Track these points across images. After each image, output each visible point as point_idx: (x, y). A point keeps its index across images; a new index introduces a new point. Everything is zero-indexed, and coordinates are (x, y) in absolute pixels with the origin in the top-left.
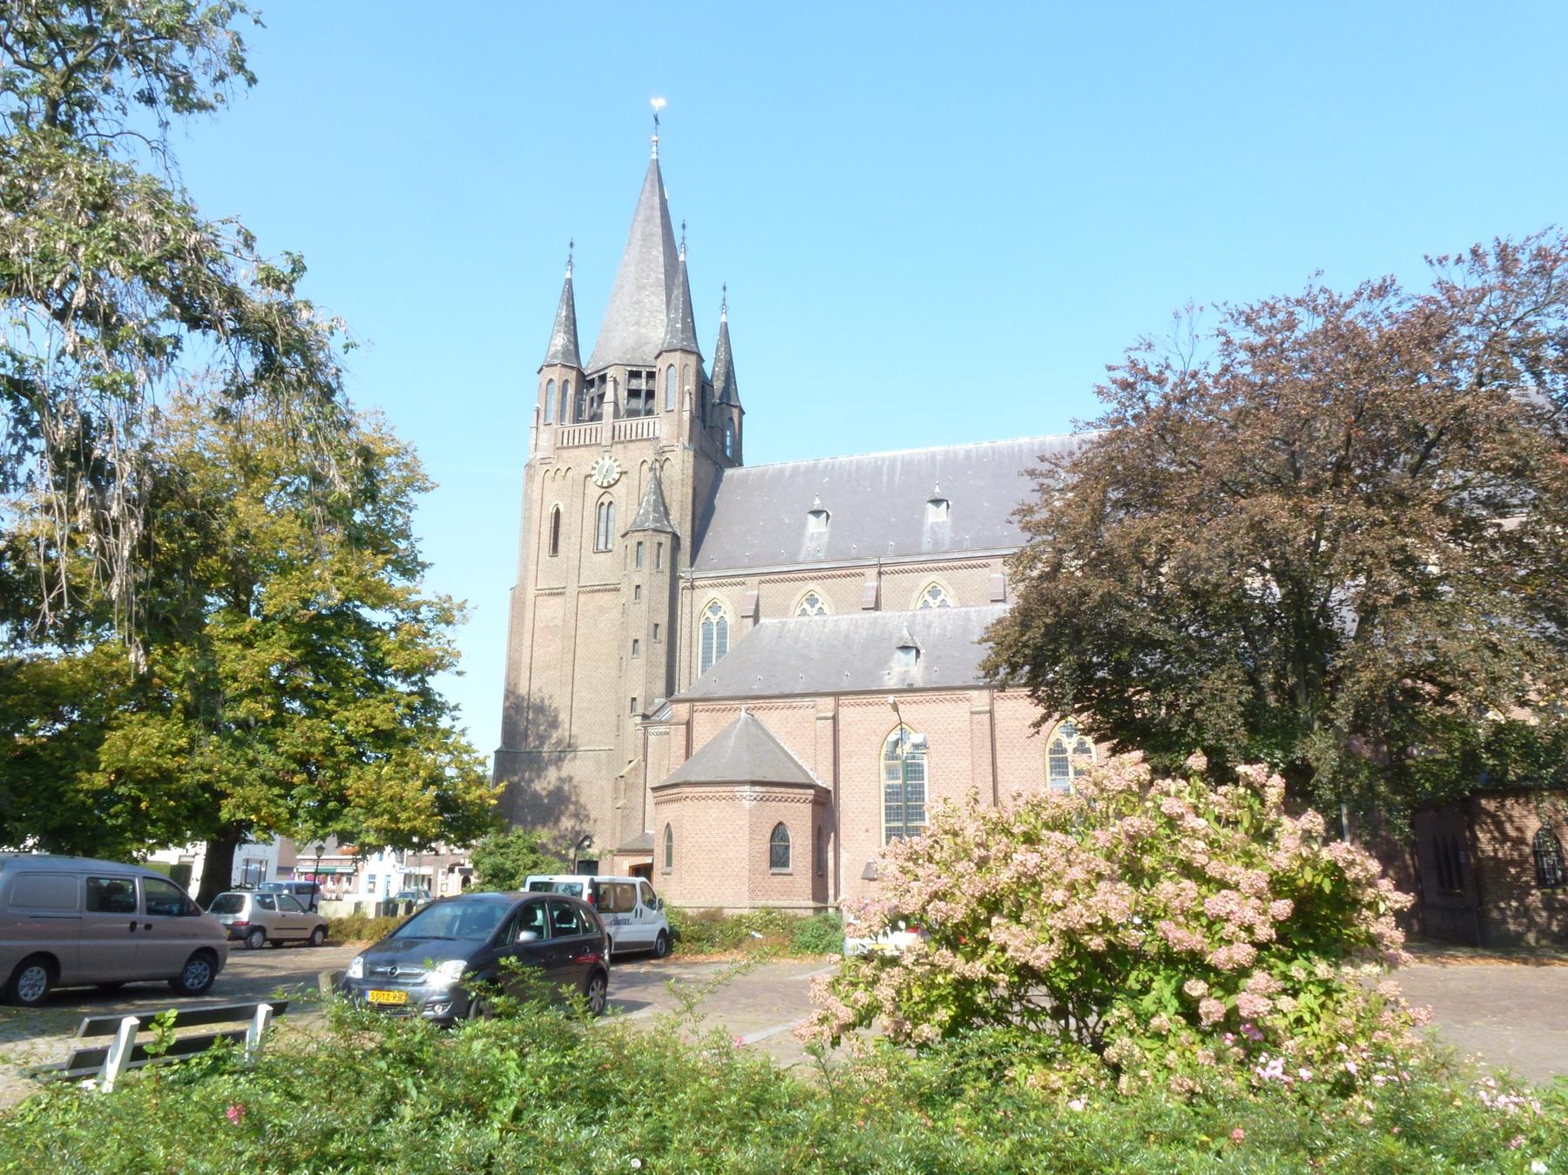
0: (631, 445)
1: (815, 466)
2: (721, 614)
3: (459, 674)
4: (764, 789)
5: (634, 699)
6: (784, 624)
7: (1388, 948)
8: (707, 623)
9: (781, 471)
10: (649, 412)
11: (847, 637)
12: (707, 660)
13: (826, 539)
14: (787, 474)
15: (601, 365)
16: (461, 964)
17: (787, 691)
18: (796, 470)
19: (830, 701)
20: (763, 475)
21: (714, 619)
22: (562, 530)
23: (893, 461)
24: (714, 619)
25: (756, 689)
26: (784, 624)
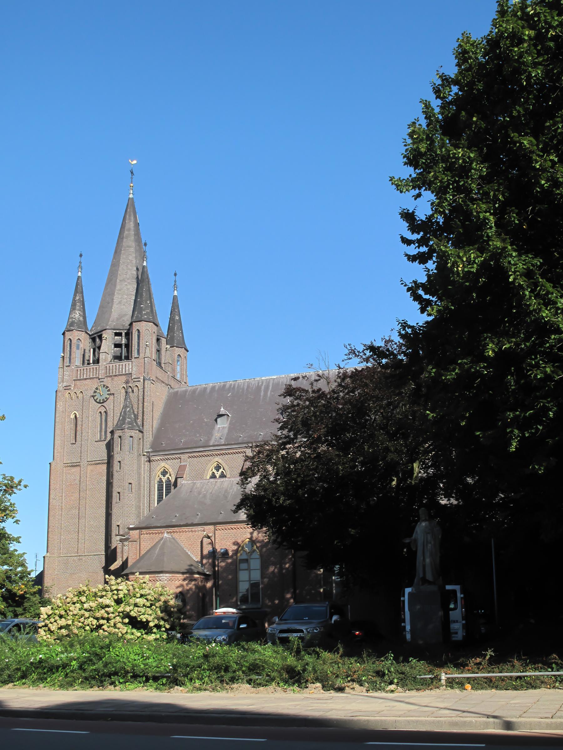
0: (116, 378)
1: (224, 386)
2: (168, 476)
3: (17, 522)
4: (171, 575)
5: (118, 526)
6: (195, 484)
7: (191, 637)
8: (161, 481)
9: (205, 389)
10: (127, 358)
11: (226, 491)
12: (160, 498)
13: (226, 431)
14: (208, 390)
15: (99, 329)
16: (34, 568)
17: (190, 522)
18: (213, 388)
19: (212, 527)
20: (194, 391)
21: (164, 479)
22: (74, 432)
23: (268, 381)
24: (164, 479)
25: (174, 521)
26: (195, 484)
